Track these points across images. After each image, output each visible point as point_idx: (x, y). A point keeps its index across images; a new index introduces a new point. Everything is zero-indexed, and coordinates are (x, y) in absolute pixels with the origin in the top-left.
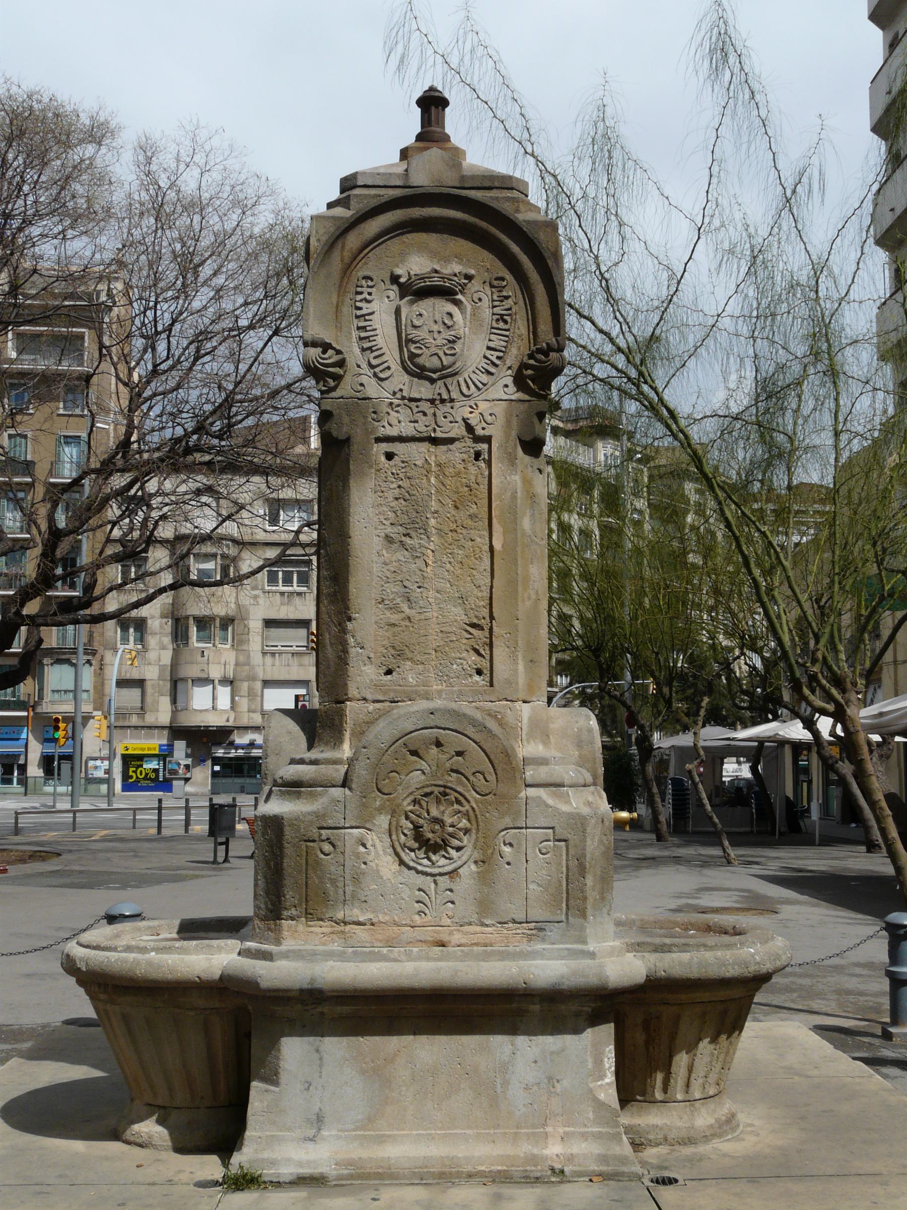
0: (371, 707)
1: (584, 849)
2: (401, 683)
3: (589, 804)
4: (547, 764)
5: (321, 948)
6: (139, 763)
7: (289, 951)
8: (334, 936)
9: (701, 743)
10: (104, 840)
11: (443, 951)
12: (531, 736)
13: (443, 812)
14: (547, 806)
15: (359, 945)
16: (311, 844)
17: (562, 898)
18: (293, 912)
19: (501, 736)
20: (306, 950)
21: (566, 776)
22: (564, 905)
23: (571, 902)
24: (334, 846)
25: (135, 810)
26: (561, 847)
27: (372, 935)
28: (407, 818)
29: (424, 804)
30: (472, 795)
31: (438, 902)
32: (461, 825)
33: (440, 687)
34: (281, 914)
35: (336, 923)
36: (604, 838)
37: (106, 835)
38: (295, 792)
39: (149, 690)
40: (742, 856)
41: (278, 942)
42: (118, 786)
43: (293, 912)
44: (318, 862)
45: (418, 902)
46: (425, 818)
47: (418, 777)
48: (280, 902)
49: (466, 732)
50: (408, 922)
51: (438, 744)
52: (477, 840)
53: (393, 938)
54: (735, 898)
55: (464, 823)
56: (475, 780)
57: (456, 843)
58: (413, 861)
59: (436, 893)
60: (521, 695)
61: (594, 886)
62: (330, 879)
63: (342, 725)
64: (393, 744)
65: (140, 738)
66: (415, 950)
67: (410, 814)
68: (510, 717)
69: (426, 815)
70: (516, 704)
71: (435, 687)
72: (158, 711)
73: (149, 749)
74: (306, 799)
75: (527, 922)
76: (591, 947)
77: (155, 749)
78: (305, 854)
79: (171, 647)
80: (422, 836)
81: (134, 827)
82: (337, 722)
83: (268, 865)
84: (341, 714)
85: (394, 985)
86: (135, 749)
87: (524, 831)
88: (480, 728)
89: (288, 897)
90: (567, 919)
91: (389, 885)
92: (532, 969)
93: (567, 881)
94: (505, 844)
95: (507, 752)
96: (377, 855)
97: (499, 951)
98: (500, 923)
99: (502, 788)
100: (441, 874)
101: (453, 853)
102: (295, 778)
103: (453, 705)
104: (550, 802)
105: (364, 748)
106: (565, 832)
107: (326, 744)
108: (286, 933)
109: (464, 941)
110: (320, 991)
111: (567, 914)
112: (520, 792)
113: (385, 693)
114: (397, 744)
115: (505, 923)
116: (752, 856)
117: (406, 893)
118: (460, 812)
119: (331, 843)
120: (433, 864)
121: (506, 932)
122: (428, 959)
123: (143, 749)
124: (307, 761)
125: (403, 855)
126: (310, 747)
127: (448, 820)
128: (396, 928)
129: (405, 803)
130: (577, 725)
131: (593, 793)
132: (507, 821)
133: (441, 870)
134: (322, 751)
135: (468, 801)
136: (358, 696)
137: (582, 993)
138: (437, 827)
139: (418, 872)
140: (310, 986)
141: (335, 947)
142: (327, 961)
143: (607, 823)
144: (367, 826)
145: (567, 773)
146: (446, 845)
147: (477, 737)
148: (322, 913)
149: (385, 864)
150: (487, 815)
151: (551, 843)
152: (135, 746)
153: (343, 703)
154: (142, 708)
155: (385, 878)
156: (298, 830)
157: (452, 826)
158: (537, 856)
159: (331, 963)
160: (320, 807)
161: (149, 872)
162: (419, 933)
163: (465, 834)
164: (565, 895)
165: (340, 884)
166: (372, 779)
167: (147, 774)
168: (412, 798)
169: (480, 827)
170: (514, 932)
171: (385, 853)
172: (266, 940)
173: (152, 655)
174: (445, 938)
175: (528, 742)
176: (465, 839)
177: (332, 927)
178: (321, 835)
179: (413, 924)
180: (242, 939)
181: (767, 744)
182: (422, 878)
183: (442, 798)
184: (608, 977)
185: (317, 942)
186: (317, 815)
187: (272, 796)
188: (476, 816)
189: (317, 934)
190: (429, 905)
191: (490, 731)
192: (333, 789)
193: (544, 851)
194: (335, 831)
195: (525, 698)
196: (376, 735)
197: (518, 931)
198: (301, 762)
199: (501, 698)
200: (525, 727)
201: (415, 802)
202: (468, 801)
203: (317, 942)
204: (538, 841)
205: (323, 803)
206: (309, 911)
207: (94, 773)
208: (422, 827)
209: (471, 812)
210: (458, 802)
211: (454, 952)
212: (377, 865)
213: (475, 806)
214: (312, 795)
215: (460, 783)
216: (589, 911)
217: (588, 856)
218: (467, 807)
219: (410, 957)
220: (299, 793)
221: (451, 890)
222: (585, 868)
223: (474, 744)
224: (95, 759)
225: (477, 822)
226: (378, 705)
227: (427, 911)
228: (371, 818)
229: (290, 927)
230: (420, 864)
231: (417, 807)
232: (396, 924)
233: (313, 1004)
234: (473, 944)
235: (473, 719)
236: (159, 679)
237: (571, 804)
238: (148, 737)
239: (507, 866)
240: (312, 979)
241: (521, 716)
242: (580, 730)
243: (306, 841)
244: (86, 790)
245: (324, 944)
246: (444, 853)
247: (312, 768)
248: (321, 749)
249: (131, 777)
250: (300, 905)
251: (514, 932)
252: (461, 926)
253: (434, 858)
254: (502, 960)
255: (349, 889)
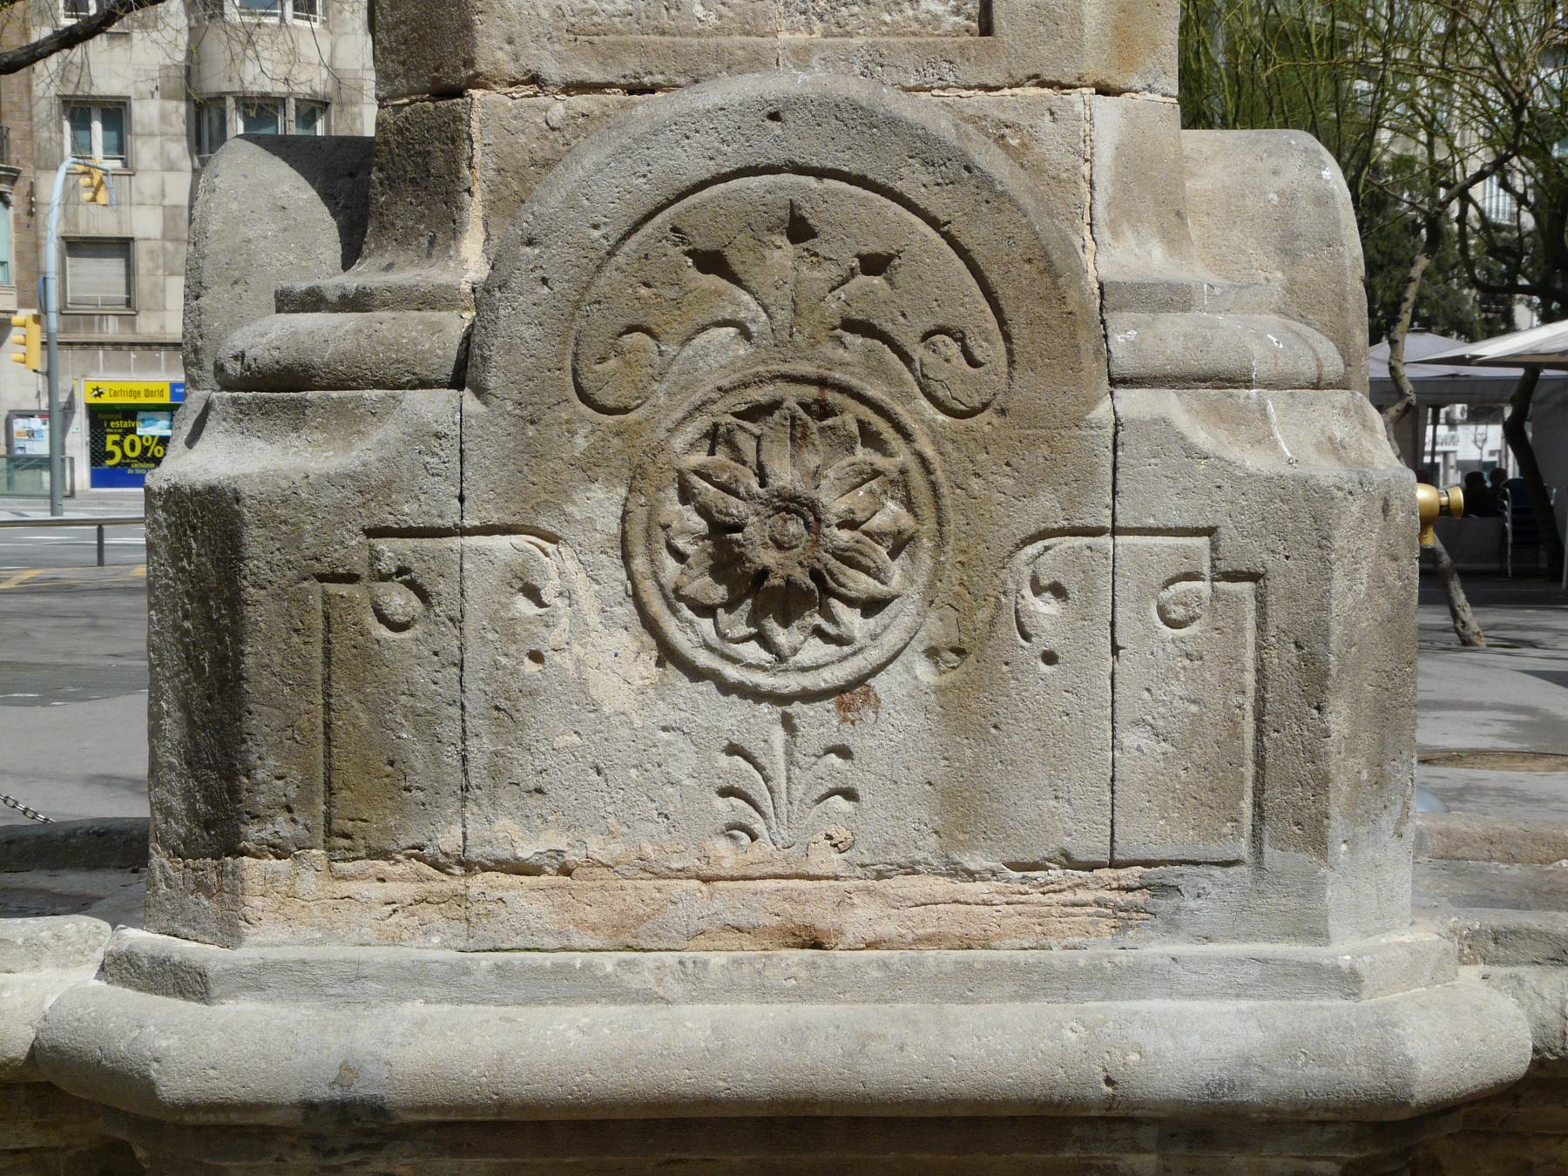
0: (559, 108)
1: (1325, 608)
2: (665, 21)
3: (1335, 448)
4: (1186, 306)
5: (381, 954)
6: (126, 424)
7: (265, 967)
8: (430, 912)
9: (1409, 372)
10: (28, 589)
11: (814, 965)
12: (1124, 212)
13: (816, 475)
14: (1191, 452)
15: (519, 941)
16: (344, 589)
17: (1241, 779)
18: (282, 827)
19: (1025, 200)
20: (326, 963)
21: (1256, 349)
22: (1247, 804)
23: (1274, 794)
24: (423, 595)
25: (100, 525)
26: (1240, 600)
27: (564, 907)
28: (686, 495)
29: (747, 446)
30: (920, 413)
31: (798, 792)
32: (879, 522)
33: (802, 37)
34: (238, 836)
35: (435, 865)
36: (1390, 566)
37: (33, 580)
38: (286, 407)
39: (143, 263)
40: (1494, 627)
41: (230, 933)
42: (82, 473)
43: (282, 827)
44: (368, 655)
45: (725, 792)
46: (750, 497)
47: (724, 347)
48: (234, 793)
49: (899, 186)
50: (691, 862)
51: (799, 230)
52: (937, 574)
53: (640, 920)
54: (1498, 728)
55: (890, 514)
56: (929, 357)
57: (861, 584)
58: (708, 647)
59: (791, 761)
60: (1094, 68)
61: (1355, 735)
62: (413, 710)
63: (455, 174)
64: (635, 228)
65: (128, 369)
66: (717, 959)
67: (695, 479)
68: (1051, 142)
69: (754, 484)
70: (1075, 95)
71: (785, 36)
72: (164, 308)
73: (148, 393)
74: (323, 427)
75: (1114, 864)
76: (1342, 950)
77: (161, 393)
78: (319, 624)
79: (187, 164)
80: (741, 559)
81: (101, 562)
82: (438, 164)
83: (191, 661)
84: (453, 135)
85: (641, 1086)
86: (116, 394)
87: (1105, 541)
88: (952, 170)
89: (261, 775)
90: (1258, 852)
91: (624, 732)
92: (1136, 1033)
93: (1259, 718)
94: (1037, 590)
95: (1046, 255)
96: (581, 630)
97: (1015, 966)
98: (1016, 866)
99: (1029, 389)
100: (808, 696)
101: (850, 618)
102: (287, 356)
103: (854, 88)
104: (1202, 437)
105: (530, 242)
106: (1255, 545)
107: (403, 241)
108: (257, 902)
109: (888, 929)
110: (377, 1109)
111: (1256, 837)
112: (1091, 403)
113: (607, 57)
114: (648, 228)
115: (1035, 866)
116: (1519, 628)
117: (684, 761)
118: (876, 473)
119: (413, 585)
120: (781, 658)
121: (1036, 896)
122: (763, 993)
123: (136, 394)
124: (332, 296)
125: (671, 627)
126: (348, 262)
127: (835, 504)
128: (648, 885)
129: (679, 443)
130: (1281, 182)
131: (1346, 411)
132: (1046, 507)
133: (810, 681)
134: (389, 267)
135: (906, 436)
136: (511, 69)
137: (1312, 1116)
138: (795, 527)
139: (726, 687)
140: (337, 1094)
141: (434, 950)
142: (401, 999)
143: (1400, 517)
144: (544, 523)
145: (1259, 336)
146: (827, 592)
147: (936, 203)
148: (385, 830)
149: (609, 659)
150: (975, 484)
151: (1203, 587)
152: (117, 387)
153: (458, 92)
154: (129, 303)
155: (607, 710)
156: (295, 541)
157: (849, 524)
158: (1152, 631)
159: (415, 1008)
160: (372, 457)
161: (114, 662)
162: (726, 902)
163: (893, 554)
164: (1249, 770)
165: (450, 731)
166: (560, 356)
167: (145, 449)
168: (702, 423)
169: (950, 528)
170: (1068, 896)
171: (608, 619)
172: (193, 922)
173: (147, 183)
174: (822, 917)
175: (1116, 234)
176: (896, 570)
177: (422, 878)
178: (375, 557)
179: (707, 871)
180: (118, 917)
181: (1547, 373)
182: (740, 708)
183: (814, 426)
184: (1410, 1062)
185: (368, 933)
186: (361, 484)
187: (210, 424)
188: (934, 487)
189: (367, 904)
190: (767, 805)
191: (986, 182)
192: (420, 394)
193: (1178, 613)
194: (427, 543)
195: (1103, 76)
196: (570, 197)
197: (1082, 895)
198: (313, 301)
199: (1020, 75)
200: (1103, 180)
201: (714, 437)
202: (906, 436)
203: (368, 933)
204: (1157, 578)
205: (383, 444)
206: (338, 824)
207: (28, 445)
208: (739, 528)
209: (917, 479)
210: (870, 438)
211: (856, 967)
212: (579, 662)
213: (929, 452)
214: (349, 421)
215: (878, 370)
216: (1337, 827)
217: (1337, 631)
218: (903, 456)
219: (698, 986)
220: (300, 408)
221: (844, 752)
222: (1326, 674)
223: (928, 230)
224: (28, 415)
225: (939, 509)
226: (582, 102)
227: (759, 826)
228: (556, 497)
229: (271, 880)
230: (734, 660)
231: (722, 456)
232: (650, 871)
233: (352, 1148)
234: (919, 941)
235: (926, 139)
236: (164, 237)
237: (1275, 446)
238: (143, 366)
239: (1044, 668)
240: (345, 1067)
241: (1088, 139)
242: (1288, 198)
243: (322, 578)
244: (10, 483)
245: (395, 940)
246: (818, 620)
247: (349, 320)
248: (387, 258)
249: (111, 455)
250: (309, 802)
251: (1068, 896)
252: (880, 876)
253: (782, 637)
254: (1025, 998)
255: (481, 748)
